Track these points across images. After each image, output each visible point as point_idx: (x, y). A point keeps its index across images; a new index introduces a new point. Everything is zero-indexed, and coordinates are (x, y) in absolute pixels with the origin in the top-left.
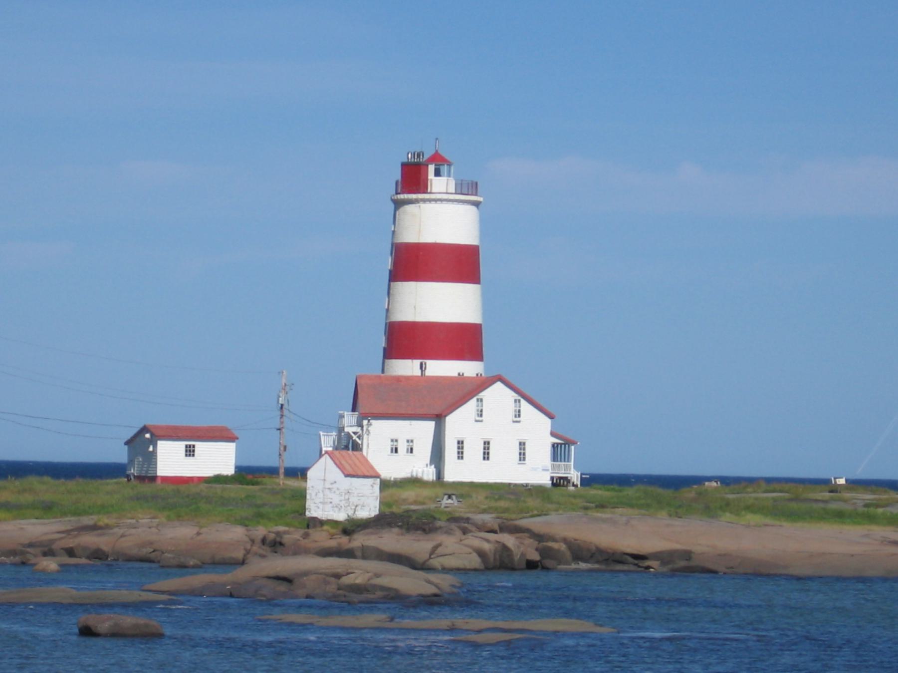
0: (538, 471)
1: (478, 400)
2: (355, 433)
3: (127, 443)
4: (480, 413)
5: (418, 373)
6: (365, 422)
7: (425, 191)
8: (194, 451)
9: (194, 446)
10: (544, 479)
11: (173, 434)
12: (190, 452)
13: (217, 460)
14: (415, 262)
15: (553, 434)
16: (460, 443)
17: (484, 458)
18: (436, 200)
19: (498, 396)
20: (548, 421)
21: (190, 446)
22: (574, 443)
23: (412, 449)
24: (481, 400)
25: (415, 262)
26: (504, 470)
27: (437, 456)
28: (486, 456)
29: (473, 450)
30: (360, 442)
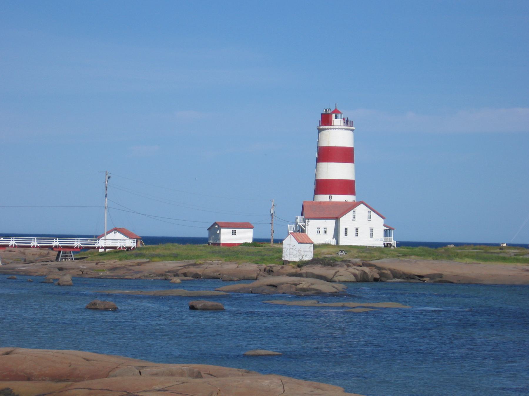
6: (307, 221)
11: (227, 226)
12: (234, 233)
13: (245, 236)
14: (326, 155)
15: (384, 225)
16: (346, 229)
18: (336, 129)
19: (361, 210)
20: (382, 221)
25: (326, 155)
27: (336, 234)
28: (357, 235)
29: (351, 232)
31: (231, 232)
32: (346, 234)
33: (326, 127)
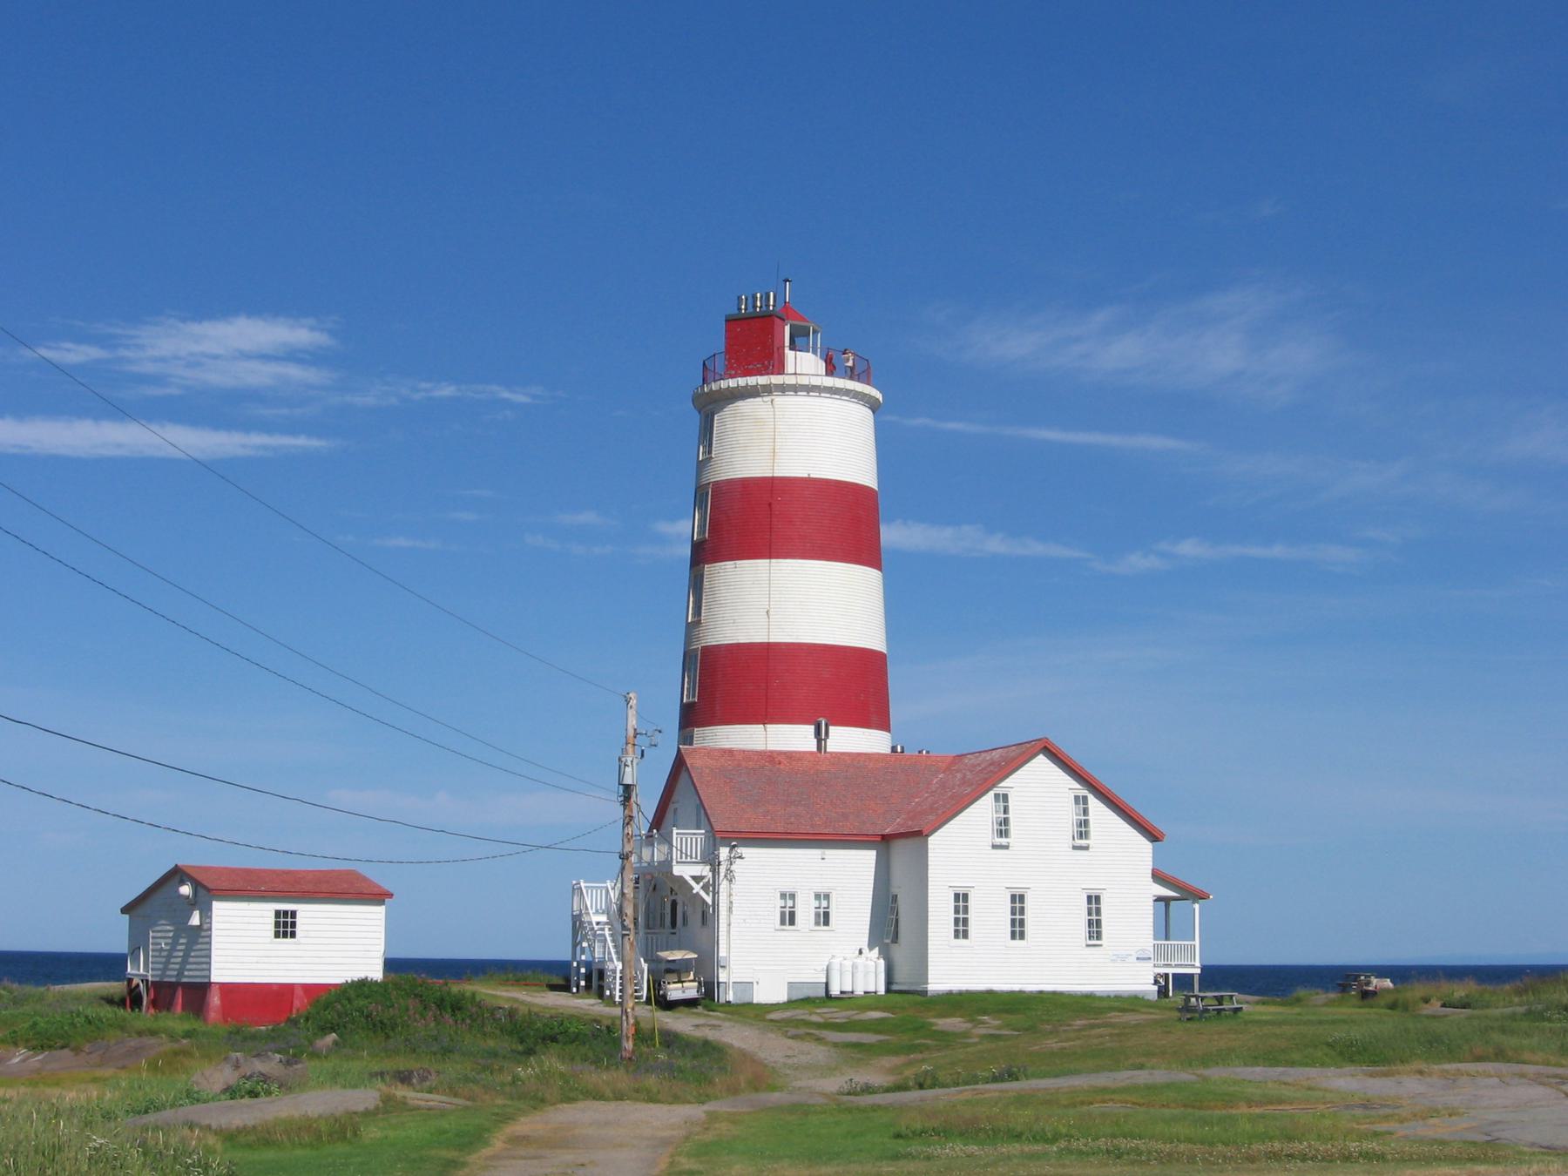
0: (1126, 964)
1: (997, 796)
2: (697, 879)
3: (125, 910)
4: (1003, 828)
5: (812, 745)
6: (724, 852)
7: (780, 370)
8: (294, 925)
9: (294, 914)
10: (1139, 980)
11: (247, 887)
12: (285, 927)
13: (342, 946)
14: (754, 520)
15: (1158, 877)
16: (961, 899)
17: (1013, 936)
18: (796, 389)
19: (1040, 788)
20: (1143, 847)
21: (286, 913)
22: (1199, 896)
23: (827, 915)
24: (1005, 797)
25: (754, 520)
26: (1054, 963)
27: (893, 922)
28: (1018, 930)
29: (990, 916)
30: (709, 900)
31: (271, 919)
32: (961, 929)
33: (762, 380)
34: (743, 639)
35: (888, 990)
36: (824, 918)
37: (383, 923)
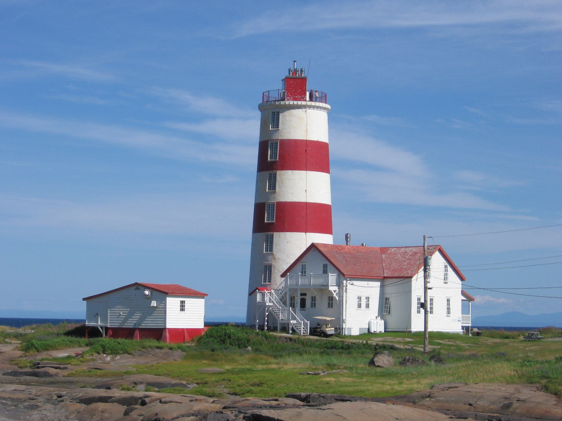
2: (335, 291)
34: (297, 200)
35: (385, 331)
36: (368, 306)
37: (204, 305)
